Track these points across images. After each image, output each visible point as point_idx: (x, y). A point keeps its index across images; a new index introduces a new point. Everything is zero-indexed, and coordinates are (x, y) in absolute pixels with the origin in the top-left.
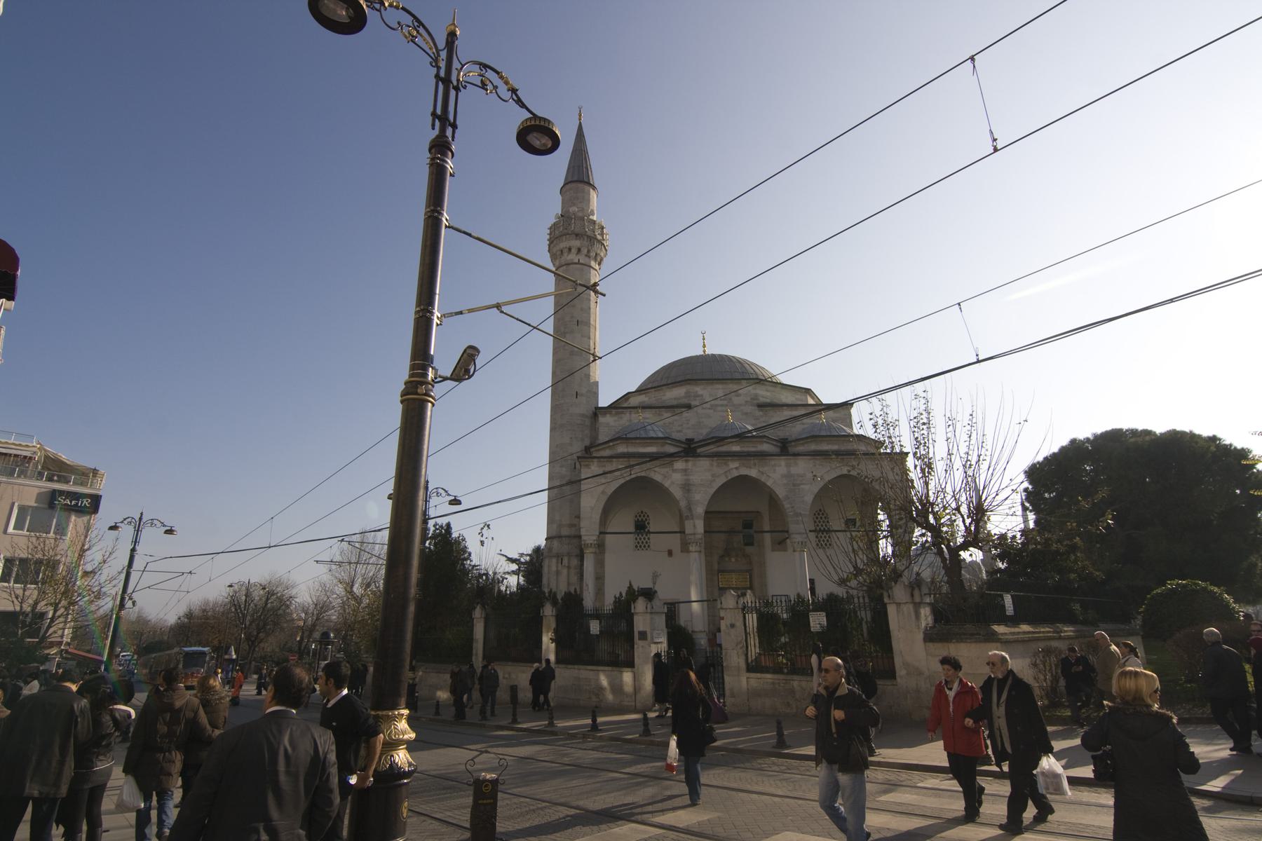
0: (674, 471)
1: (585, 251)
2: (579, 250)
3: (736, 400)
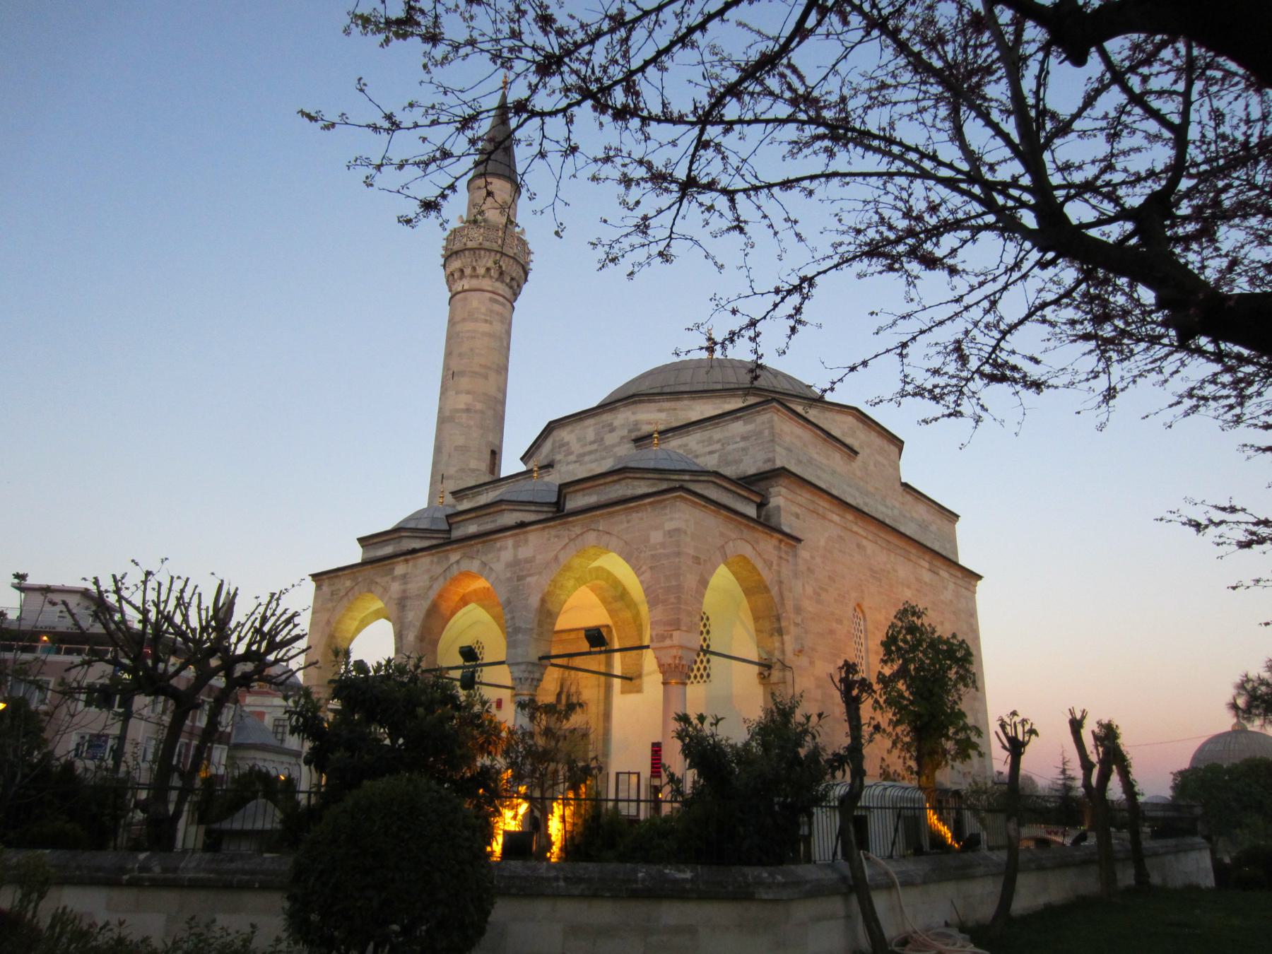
0: (394, 579)
1: (468, 271)
2: (462, 271)
3: (610, 439)
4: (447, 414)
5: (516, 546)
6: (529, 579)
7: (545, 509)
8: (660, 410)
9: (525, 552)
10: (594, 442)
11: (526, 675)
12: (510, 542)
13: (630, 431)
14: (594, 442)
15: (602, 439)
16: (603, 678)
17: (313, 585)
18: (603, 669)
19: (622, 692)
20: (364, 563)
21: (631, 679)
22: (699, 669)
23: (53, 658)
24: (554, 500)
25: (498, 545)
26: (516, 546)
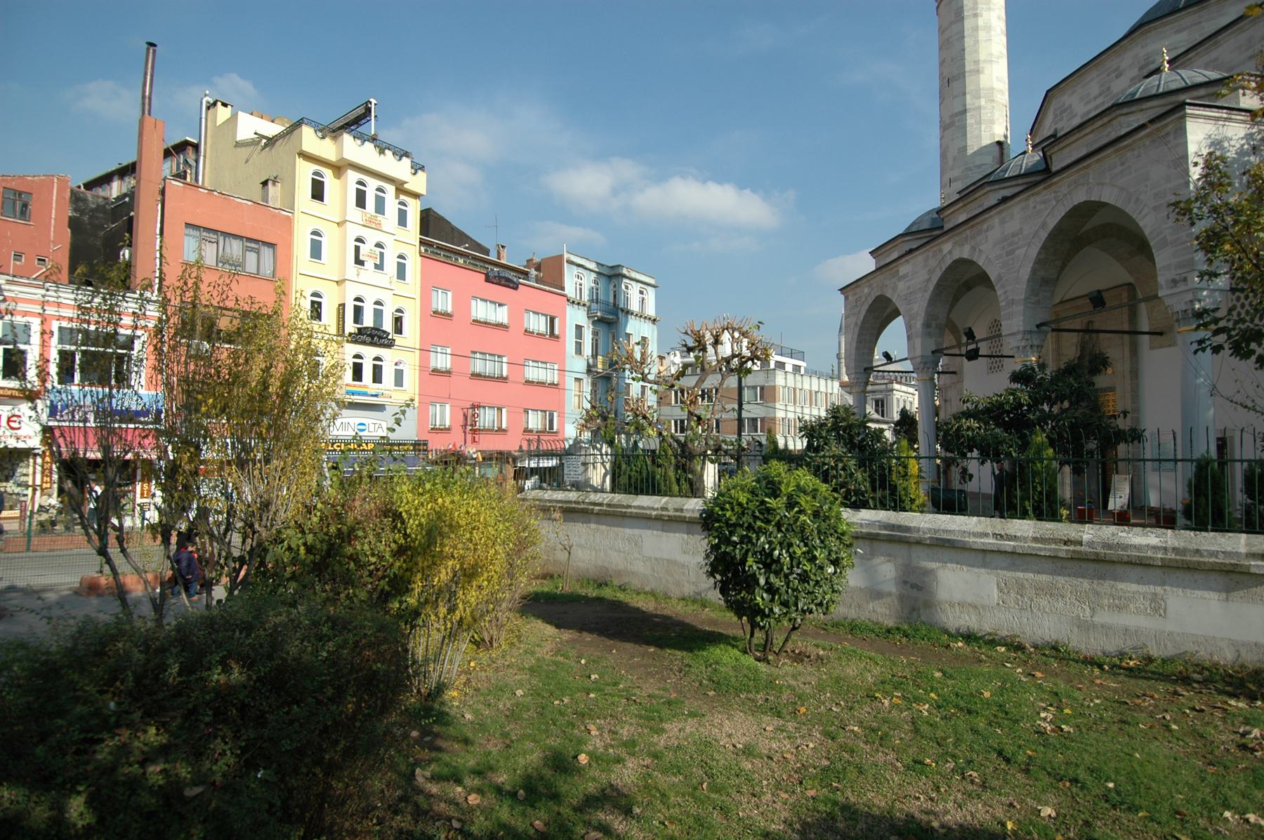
0: (900, 279)
4: (948, 121)
5: (1003, 222)
6: (1017, 252)
7: (1020, 181)
8: (1178, 32)
9: (1012, 226)
10: (1100, 95)
11: (1023, 343)
12: (996, 221)
13: (1141, 69)
14: (1100, 95)
15: (1109, 89)
16: (1126, 337)
17: (842, 297)
18: (1126, 327)
19: (1151, 348)
20: (877, 270)
21: (1161, 334)
22: (1243, 306)
23: (73, 348)
24: (1044, 166)
25: (985, 226)
26: (1003, 222)
